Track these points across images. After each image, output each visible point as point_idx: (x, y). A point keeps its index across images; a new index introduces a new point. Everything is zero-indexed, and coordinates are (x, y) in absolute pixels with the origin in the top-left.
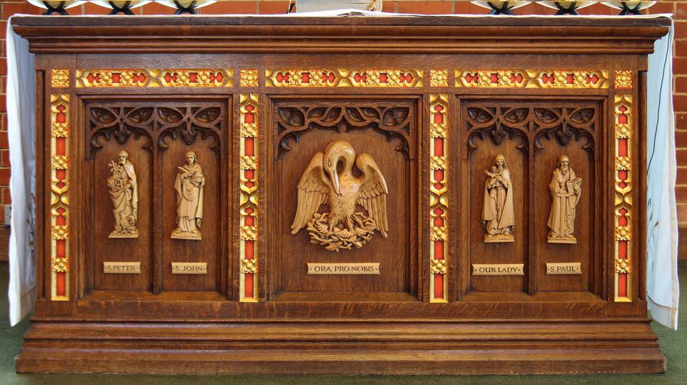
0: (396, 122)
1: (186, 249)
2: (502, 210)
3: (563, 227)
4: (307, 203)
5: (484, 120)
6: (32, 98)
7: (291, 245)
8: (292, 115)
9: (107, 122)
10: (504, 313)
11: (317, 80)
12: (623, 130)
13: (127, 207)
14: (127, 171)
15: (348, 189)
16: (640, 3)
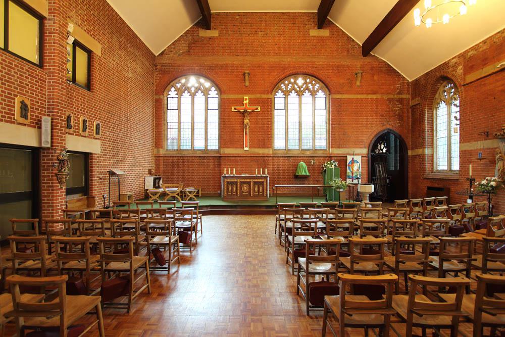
0: (249, 183)
1: (234, 192)
2: (256, 189)
3: (261, 190)
4: (243, 189)
5: (255, 183)
6: (410, 165)
7: (241, 192)
8: (402, 148)
9: (229, 183)
10: (257, 197)
11: (243, 180)
12: (265, 184)
13: (230, 189)
14: (230, 187)
15: (245, 188)
16: (113, 329)
